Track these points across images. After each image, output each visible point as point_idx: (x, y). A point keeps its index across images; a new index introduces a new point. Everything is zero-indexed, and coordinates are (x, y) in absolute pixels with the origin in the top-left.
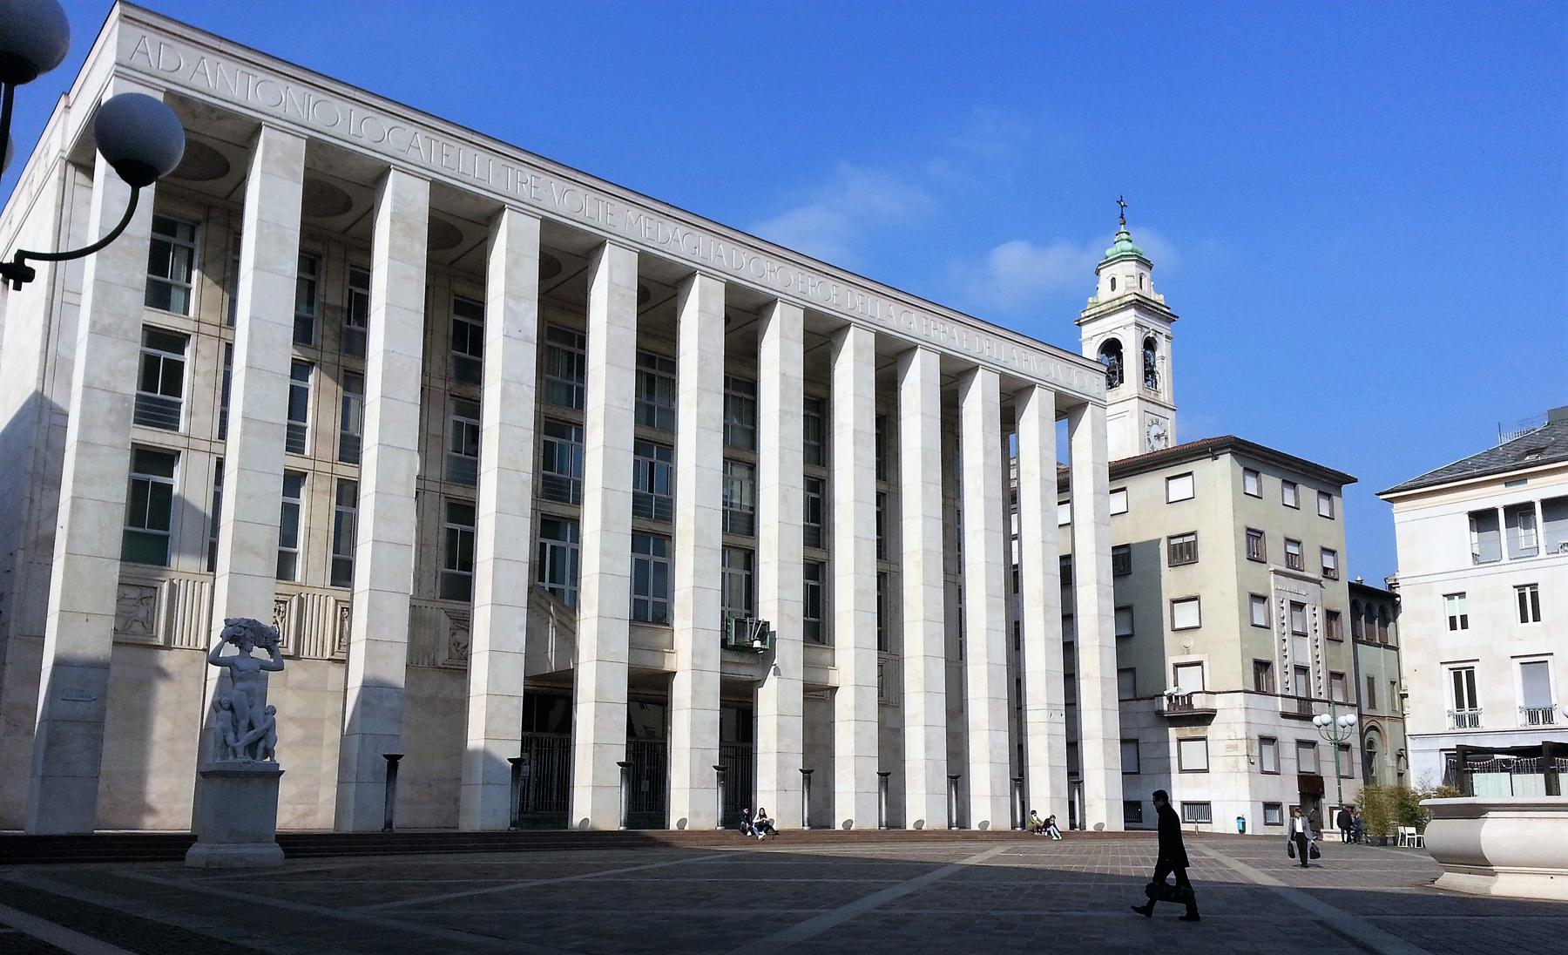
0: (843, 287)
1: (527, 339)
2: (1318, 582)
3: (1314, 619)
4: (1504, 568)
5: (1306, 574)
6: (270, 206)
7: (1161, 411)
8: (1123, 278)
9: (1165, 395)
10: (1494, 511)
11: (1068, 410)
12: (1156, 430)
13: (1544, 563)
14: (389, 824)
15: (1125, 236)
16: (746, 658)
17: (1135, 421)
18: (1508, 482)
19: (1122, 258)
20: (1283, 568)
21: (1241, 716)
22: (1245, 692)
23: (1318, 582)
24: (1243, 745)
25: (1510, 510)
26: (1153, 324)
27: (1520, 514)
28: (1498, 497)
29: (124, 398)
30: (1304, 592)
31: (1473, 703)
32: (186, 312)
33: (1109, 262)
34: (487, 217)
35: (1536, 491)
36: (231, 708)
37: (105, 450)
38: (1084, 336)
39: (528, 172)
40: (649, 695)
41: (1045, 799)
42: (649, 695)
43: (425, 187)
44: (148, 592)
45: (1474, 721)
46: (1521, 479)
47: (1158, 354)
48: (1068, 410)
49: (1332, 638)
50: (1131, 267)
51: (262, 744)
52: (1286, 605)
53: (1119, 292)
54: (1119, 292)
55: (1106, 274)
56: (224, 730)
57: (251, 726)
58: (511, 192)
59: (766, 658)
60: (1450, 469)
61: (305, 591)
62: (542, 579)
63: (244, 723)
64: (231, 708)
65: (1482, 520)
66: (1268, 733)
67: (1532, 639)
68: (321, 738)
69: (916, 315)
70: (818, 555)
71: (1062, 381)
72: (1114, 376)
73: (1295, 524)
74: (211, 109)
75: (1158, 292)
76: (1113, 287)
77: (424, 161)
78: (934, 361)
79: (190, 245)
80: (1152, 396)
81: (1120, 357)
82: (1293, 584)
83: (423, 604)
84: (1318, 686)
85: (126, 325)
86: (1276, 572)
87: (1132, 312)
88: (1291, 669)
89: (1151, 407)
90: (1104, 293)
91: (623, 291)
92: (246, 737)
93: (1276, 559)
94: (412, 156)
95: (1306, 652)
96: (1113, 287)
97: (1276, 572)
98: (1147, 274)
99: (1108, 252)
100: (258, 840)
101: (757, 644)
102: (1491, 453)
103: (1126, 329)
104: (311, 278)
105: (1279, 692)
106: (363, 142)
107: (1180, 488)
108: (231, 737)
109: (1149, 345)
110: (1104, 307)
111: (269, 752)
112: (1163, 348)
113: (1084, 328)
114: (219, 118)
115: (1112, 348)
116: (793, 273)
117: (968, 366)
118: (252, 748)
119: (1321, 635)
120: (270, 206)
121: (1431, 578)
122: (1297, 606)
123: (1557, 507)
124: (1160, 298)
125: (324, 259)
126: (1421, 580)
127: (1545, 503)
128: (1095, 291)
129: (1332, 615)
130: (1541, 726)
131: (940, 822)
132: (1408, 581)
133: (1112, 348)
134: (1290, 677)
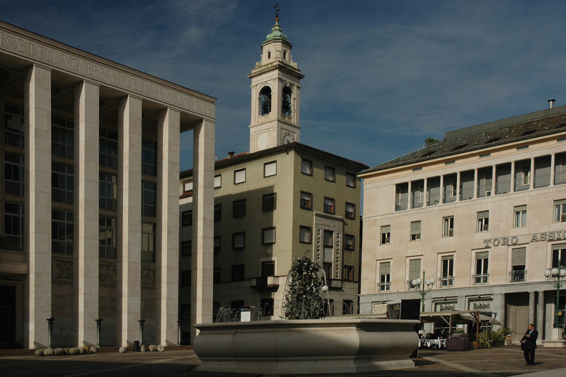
2: (342, 220)
5: (336, 216)
7: (292, 129)
9: (294, 120)
11: (190, 124)
13: (425, 210)
15: (277, 28)
17: (275, 134)
18: (415, 168)
19: (275, 40)
20: (322, 213)
23: (342, 220)
28: (408, 176)
30: (336, 226)
31: (451, 274)
33: (268, 42)
38: (253, 84)
41: (167, 331)
45: (451, 283)
46: (419, 168)
47: (292, 97)
48: (190, 124)
53: (272, 60)
54: (272, 60)
55: (266, 49)
60: (392, 162)
65: (401, 188)
69: (82, 61)
71: (186, 106)
72: (265, 109)
73: (331, 190)
78: (96, 91)
80: (287, 119)
81: (270, 97)
82: (327, 222)
86: (317, 215)
87: (277, 72)
89: (285, 126)
90: (265, 60)
93: (318, 208)
102: (413, 154)
103: (272, 79)
107: (271, 170)
109: (286, 91)
110: (263, 68)
112: (295, 91)
113: (253, 80)
115: (266, 91)
119: (340, 247)
121: (377, 218)
124: (294, 65)
128: (259, 59)
132: (367, 219)
133: (266, 91)
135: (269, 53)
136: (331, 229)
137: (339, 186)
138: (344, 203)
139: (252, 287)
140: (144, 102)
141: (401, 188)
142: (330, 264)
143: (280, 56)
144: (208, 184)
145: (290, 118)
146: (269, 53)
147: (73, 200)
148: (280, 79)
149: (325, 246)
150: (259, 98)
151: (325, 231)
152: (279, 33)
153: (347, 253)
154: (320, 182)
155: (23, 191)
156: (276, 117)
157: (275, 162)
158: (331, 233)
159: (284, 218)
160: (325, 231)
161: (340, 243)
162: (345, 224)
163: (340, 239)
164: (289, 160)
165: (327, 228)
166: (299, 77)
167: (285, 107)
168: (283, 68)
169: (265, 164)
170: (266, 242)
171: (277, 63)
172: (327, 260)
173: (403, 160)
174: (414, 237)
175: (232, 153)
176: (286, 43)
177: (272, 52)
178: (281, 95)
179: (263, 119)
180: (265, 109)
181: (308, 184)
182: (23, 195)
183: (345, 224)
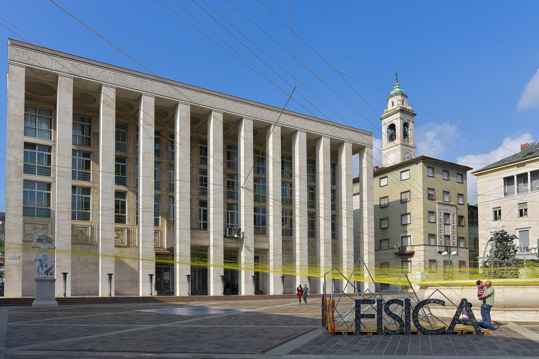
0: (268, 111)
1: (151, 138)
2: (455, 206)
3: (453, 220)
4: (515, 197)
5: (451, 203)
6: (65, 101)
7: (410, 149)
8: (394, 103)
10: (512, 177)
12: (407, 155)
14: (65, 294)
15: (397, 86)
16: (234, 241)
18: (519, 166)
19: (396, 94)
20: (442, 202)
21: (422, 253)
22: (424, 245)
23: (455, 206)
24: (423, 263)
25: (519, 176)
26: (407, 118)
27: (522, 178)
28: (514, 172)
29: (20, 167)
32: (51, 139)
34: (138, 99)
35: (528, 169)
36: (40, 261)
37: (15, 184)
38: (383, 123)
39: (150, 82)
40: (200, 253)
42: (200, 253)
43: (114, 90)
44: (45, 226)
46: (523, 165)
48: (358, 150)
49: (459, 225)
50: (399, 97)
51: (50, 271)
52: (442, 214)
53: (395, 107)
54: (395, 107)
55: (390, 101)
56: (38, 267)
57: (46, 266)
58: (144, 89)
59: (240, 240)
60: (499, 162)
61: (93, 224)
62: (228, 222)
63: (44, 265)
64: (40, 261)
65: (508, 180)
66: (433, 258)
67: (523, 223)
68: (478, 264)
70: (312, 210)
72: (392, 138)
74: (42, 71)
75: (409, 105)
76: (393, 105)
77: (114, 82)
78: (304, 135)
79: (50, 117)
80: (406, 143)
81: (395, 130)
83: (131, 227)
84: (453, 242)
85: (19, 144)
86: (439, 203)
88: (443, 237)
89: (406, 148)
90: (390, 107)
91: (186, 119)
92: (45, 269)
94: (110, 80)
95: (449, 230)
96: (393, 105)
97: (439, 203)
98: (405, 100)
99: (391, 93)
100: (50, 299)
101: (236, 236)
103: (397, 120)
104: (90, 124)
105: (438, 244)
106: (93, 77)
107: (405, 176)
108: (40, 269)
109: (406, 125)
111: (52, 274)
112: (411, 125)
114: (45, 74)
116: (249, 107)
117: (317, 137)
118: (47, 272)
119: (455, 225)
120: (65, 101)
122: (447, 215)
123: (536, 174)
124: (410, 108)
125: (93, 118)
126: (485, 203)
127: (531, 172)
128: (386, 107)
129: (461, 217)
130: (525, 253)
131: (280, 292)
133: (392, 127)
134: (443, 240)
135: (393, 103)
136: (449, 212)
137: (452, 183)
138: (457, 195)
139: (395, 254)
140: (331, 139)
141: (508, 180)
142: (449, 236)
143: (400, 103)
144: (370, 188)
145: (408, 142)
146: (393, 103)
147: (266, 200)
148: (401, 118)
149: (445, 224)
150: (388, 132)
151: (445, 214)
152: (398, 90)
153: (459, 228)
154: (440, 181)
155: (237, 197)
156: (400, 142)
157: (408, 170)
158: (449, 214)
159: (416, 208)
160: (445, 214)
161: (455, 222)
162: (457, 209)
163: (455, 219)
164: (418, 169)
165: (446, 212)
166: (414, 115)
167: (405, 135)
168: (402, 111)
169: (401, 172)
170: (403, 223)
171: (399, 108)
172: (446, 234)
173: (508, 160)
174: (521, 215)
175: (377, 167)
176: (404, 95)
177: (394, 103)
178: (402, 128)
179: (391, 144)
180: (392, 138)
181: (432, 183)
182: (237, 199)
183: (457, 209)
